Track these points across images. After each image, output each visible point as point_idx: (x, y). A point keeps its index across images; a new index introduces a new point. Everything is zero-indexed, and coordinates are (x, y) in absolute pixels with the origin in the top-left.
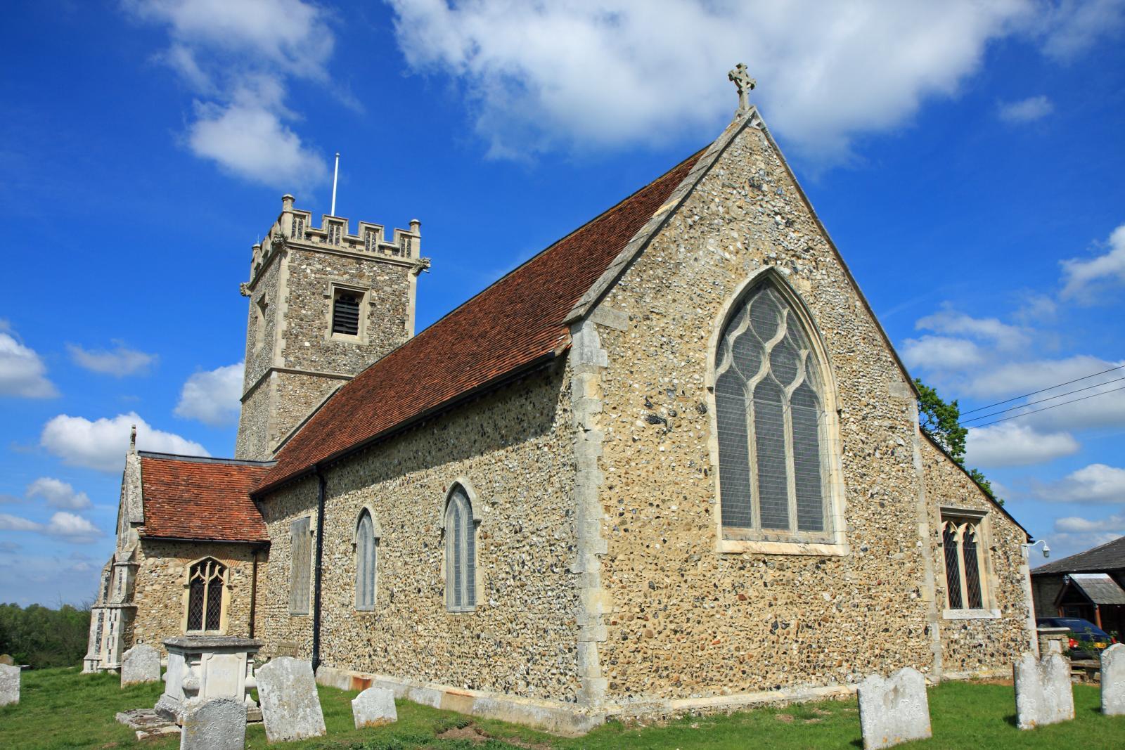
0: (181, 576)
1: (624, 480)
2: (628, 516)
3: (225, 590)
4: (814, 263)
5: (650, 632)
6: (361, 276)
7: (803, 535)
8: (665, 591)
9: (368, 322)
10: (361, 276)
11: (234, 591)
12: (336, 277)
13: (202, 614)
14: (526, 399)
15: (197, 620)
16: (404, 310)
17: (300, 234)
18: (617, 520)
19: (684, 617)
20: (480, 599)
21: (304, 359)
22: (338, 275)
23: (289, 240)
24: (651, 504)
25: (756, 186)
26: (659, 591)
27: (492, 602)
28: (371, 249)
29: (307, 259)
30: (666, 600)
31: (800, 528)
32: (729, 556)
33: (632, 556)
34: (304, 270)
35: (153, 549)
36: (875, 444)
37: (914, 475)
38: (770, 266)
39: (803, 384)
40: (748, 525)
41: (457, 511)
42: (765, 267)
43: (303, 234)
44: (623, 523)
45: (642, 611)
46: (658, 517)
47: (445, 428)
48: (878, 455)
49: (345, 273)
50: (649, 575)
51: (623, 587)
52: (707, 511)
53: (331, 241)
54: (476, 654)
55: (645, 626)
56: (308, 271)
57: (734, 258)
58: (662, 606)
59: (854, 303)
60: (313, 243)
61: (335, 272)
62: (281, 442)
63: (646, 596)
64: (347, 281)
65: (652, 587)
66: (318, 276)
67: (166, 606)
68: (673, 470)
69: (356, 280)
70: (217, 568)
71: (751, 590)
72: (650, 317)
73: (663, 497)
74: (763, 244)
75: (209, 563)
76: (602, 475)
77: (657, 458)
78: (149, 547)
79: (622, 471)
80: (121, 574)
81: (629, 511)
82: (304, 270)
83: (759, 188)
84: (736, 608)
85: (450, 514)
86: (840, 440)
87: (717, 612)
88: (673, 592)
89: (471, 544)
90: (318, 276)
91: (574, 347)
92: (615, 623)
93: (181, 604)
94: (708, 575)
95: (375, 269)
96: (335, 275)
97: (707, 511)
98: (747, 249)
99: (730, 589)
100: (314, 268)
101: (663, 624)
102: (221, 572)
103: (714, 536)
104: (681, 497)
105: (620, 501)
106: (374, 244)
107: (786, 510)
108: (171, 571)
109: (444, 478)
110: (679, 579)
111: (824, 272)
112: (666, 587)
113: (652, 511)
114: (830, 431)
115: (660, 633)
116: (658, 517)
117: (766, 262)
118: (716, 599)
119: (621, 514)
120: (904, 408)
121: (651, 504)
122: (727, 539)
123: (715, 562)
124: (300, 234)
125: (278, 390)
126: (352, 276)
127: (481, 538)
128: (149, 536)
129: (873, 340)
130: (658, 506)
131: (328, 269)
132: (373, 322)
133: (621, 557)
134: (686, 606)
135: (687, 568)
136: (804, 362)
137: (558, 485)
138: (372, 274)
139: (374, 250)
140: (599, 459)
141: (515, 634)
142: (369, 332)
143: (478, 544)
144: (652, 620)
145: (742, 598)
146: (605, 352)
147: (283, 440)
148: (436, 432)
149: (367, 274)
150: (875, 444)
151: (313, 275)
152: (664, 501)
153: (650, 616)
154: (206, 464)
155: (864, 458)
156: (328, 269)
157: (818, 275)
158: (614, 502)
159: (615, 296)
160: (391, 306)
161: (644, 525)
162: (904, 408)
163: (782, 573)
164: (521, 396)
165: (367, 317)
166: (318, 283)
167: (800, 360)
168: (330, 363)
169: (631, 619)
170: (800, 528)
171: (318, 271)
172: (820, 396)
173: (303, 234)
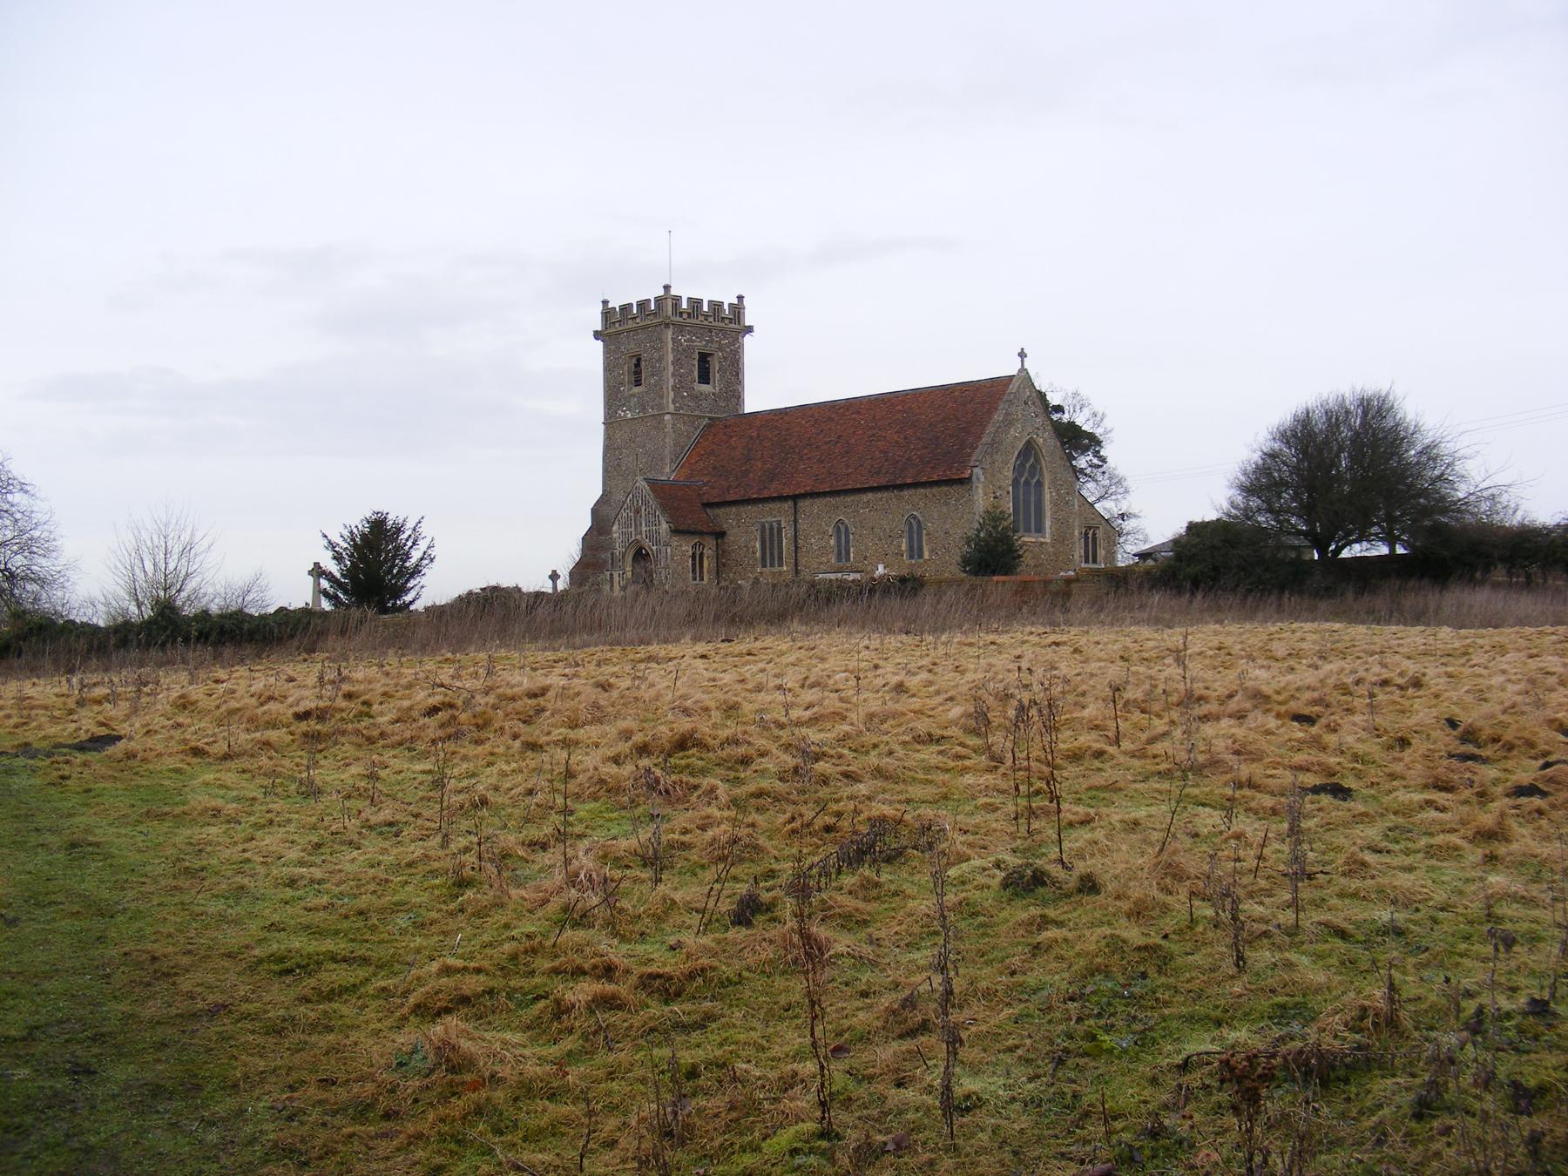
6: (712, 341)
20: (926, 556)
114: (1047, 496)
143: (924, 538)
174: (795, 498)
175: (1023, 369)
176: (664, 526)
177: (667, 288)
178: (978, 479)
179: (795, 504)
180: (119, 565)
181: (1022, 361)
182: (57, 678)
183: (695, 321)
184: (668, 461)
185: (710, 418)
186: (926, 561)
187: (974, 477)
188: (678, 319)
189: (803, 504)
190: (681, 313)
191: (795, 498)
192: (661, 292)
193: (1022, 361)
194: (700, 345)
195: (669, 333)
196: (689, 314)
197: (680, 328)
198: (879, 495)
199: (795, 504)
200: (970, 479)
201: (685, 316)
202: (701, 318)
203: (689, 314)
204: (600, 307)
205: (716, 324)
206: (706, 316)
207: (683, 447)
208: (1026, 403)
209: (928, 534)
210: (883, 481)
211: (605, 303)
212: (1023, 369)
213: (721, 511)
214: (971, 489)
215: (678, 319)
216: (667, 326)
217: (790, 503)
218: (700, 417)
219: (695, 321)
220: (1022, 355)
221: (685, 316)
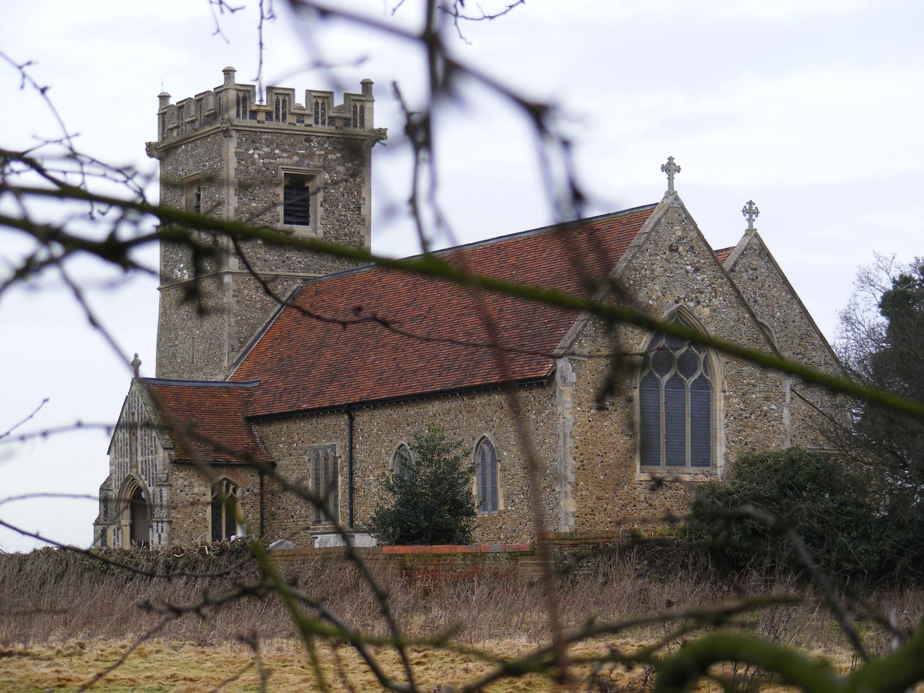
0: (204, 495)
1: (584, 443)
2: (585, 462)
3: (239, 505)
4: (713, 294)
5: (597, 522)
6: (311, 155)
7: (695, 470)
8: (605, 501)
9: (320, 210)
10: (311, 155)
11: (246, 508)
12: (286, 160)
13: (221, 528)
14: (530, 393)
15: (218, 533)
16: (359, 193)
17: (245, 112)
18: (579, 464)
19: (616, 515)
20: (501, 507)
21: (258, 258)
22: (287, 158)
23: (236, 123)
24: (598, 455)
25: (673, 249)
26: (602, 501)
27: (509, 508)
28: (320, 122)
29: (253, 142)
30: (605, 506)
31: (692, 465)
32: (643, 482)
33: (587, 483)
34: (252, 156)
35: (181, 471)
36: (752, 410)
37: (782, 429)
38: (680, 304)
39: (701, 376)
40: (684, 465)
41: (484, 453)
42: (676, 306)
43: (248, 113)
44: (583, 465)
45: (592, 511)
46: (602, 462)
47: (473, 398)
48: (753, 417)
49: (294, 155)
50: (597, 492)
51: (582, 499)
52: (631, 457)
53: (277, 117)
54: (499, 538)
55: (594, 519)
56: (256, 156)
57: (656, 303)
58: (603, 509)
59: (743, 315)
60: (259, 122)
61: (284, 155)
62: (241, 353)
63: (594, 503)
64: (296, 164)
65: (597, 498)
66: (266, 161)
67: (194, 521)
68: (611, 436)
69: (306, 161)
70: (231, 488)
71: (656, 501)
72: (601, 349)
73: (605, 451)
74: (676, 290)
75: (225, 482)
76: (572, 441)
77: (602, 430)
78: (178, 470)
79: (583, 438)
80: (161, 493)
81: (586, 459)
82: (252, 156)
83: (676, 250)
84: (647, 511)
85: (479, 453)
86: (724, 410)
87: (635, 512)
88: (610, 501)
89: (494, 475)
90: (266, 161)
91: (558, 371)
92: (578, 517)
93: (205, 519)
94: (631, 492)
95: (326, 146)
96: (283, 157)
97: (631, 457)
98: (664, 295)
99: (643, 500)
100: (262, 153)
101: (603, 517)
102: (235, 490)
103: (634, 471)
104: (616, 450)
105: (581, 454)
106: (323, 115)
107: (684, 455)
108: (196, 490)
109: (473, 431)
110: (614, 494)
111: (721, 298)
112: (606, 499)
113: (599, 459)
114: (719, 405)
115: (602, 522)
116: (602, 462)
117: (677, 302)
118: (635, 506)
119: (582, 461)
120: (778, 384)
121: (598, 455)
122: (644, 473)
123: (634, 486)
124: (245, 112)
125: (234, 296)
126: (303, 157)
127: (501, 470)
128: (180, 459)
129: (757, 339)
130: (602, 456)
131: (277, 151)
132: (327, 210)
133: (582, 483)
134: (617, 509)
135: (618, 489)
136: (702, 362)
137: (548, 445)
138: (323, 152)
139: (323, 123)
140: (571, 433)
141: (524, 525)
142: (323, 222)
143: (499, 475)
144: (597, 516)
145: (651, 505)
146: (574, 374)
147: (243, 350)
148: (465, 399)
149: (317, 153)
150: (752, 410)
151: (261, 161)
152: (605, 453)
153: (596, 514)
154: (198, 387)
155: (742, 420)
156: (277, 151)
157: (716, 302)
158: (578, 455)
159: (580, 341)
160: (345, 189)
161: (594, 466)
162: (778, 384)
163: (677, 492)
164: (527, 391)
165: (319, 204)
166: (267, 169)
167: (700, 361)
168: (284, 262)
169: (586, 515)
170: (692, 465)
171: (266, 156)
172: (713, 384)
173: (248, 113)
174: (350, 410)
175: (671, 192)
176: (162, 455)
177: (229, 73)
178: (564, 379)
179: (352, 419)
180: (477, 453)
181: (671, 180)
182: (156, 639)
183: (281, 125)
184: (226, 349)
185: (305, 280)
186: (500, 514)
187: (558, 376)
188: (249, 122)
189: (362, 418)
190: (254, 114)
191: (350, 410)
192: (220, 81)
193: (671, 180)
194: (287, 162)
195: (232, 146)
196: (269, 115)
197: (252, 137)
198: (447, 405)
199: (352, 419)
200: (551, 378)
201: (261, 116)
202: (291, 119)
203: (269, 115)
204: (156, 104)
205: (320, 127)
206: (301, 117)
207: (254, 327)
208: (673, 249)
209: (503, 470)
210: (448, 381)
211: (164, 98)
212: (671, 192)
213: (269, 430)
214: (553, 395)
215: (249, 122)
216: (226, 133)
217: (343, 420)
218: (287, 278)
219: (281, 125)
220: (670, 168)
221: (261, 116)
